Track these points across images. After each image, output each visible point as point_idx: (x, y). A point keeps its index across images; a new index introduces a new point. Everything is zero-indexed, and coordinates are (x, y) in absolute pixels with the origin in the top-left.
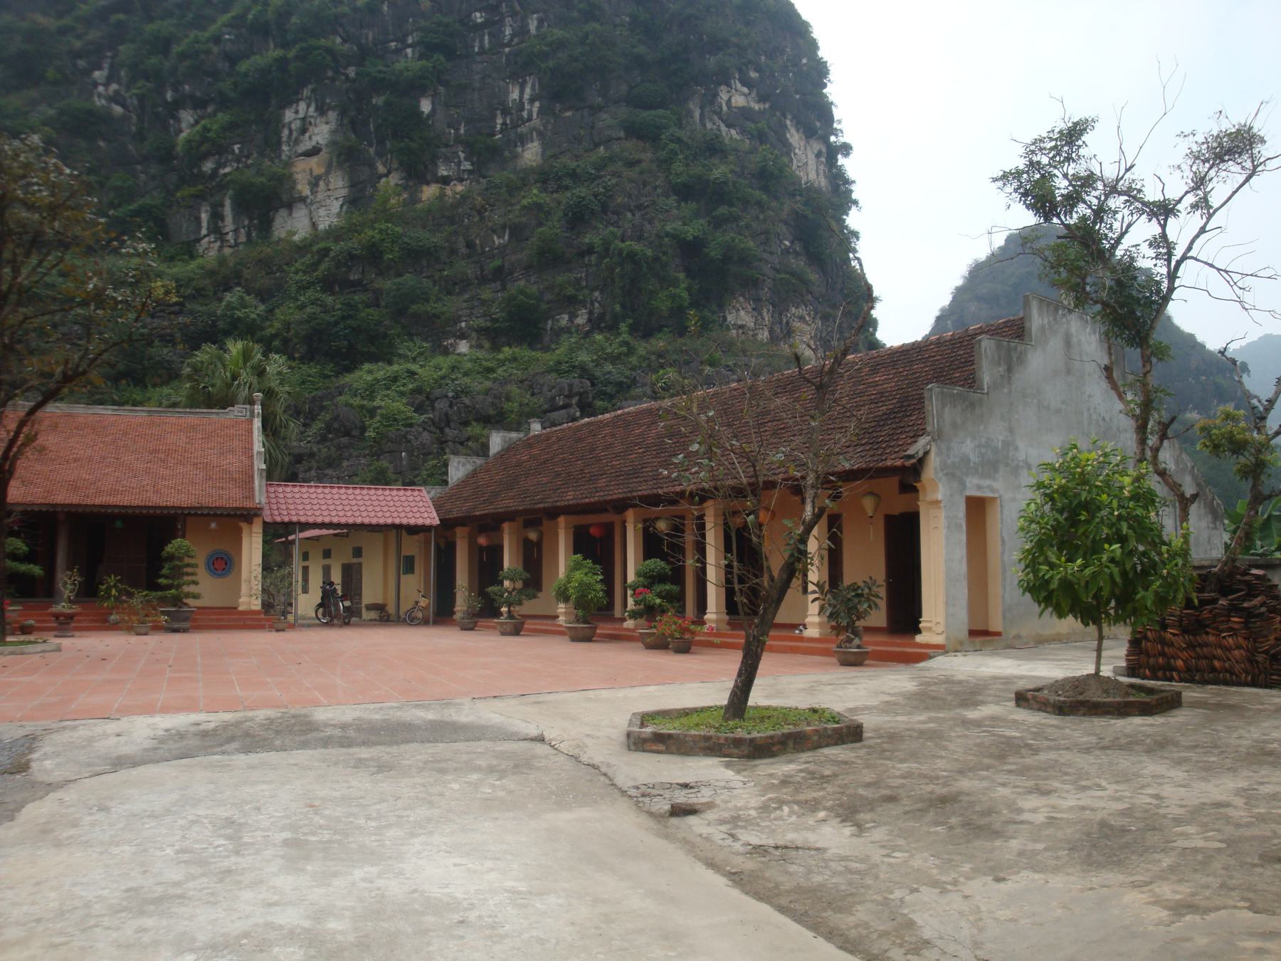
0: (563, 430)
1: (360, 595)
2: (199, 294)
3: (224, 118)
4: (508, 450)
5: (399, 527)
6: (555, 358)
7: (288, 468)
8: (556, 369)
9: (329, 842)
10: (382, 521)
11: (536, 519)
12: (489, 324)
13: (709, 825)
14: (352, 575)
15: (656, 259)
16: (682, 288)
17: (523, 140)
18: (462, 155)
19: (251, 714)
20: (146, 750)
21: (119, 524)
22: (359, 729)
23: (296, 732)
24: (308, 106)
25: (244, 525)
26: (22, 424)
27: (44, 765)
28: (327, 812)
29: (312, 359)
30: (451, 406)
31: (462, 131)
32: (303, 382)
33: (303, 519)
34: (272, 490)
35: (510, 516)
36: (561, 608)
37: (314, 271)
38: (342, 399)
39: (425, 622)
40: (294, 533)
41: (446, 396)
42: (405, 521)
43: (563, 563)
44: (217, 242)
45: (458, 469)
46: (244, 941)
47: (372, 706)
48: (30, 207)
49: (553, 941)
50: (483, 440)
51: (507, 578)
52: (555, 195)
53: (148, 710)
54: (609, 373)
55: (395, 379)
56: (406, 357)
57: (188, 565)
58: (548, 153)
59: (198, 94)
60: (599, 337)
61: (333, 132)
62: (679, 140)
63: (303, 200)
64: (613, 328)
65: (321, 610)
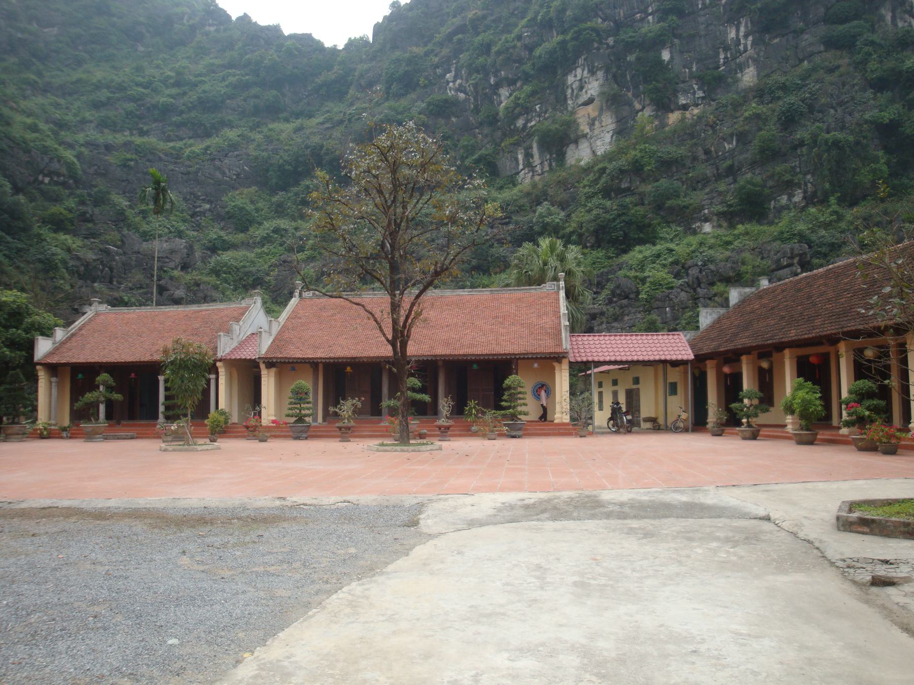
0: (786, 284)
1: (639, 411)
2: (520, 209)
3: (528, 88)
4: (744, 302)
5: (664, 362)
6: (778, 229)
7: (585, 324)
8: (781, 238)
9: (605, 585)
10: (652, 358)
11: (768, 351)
12: (725, 209)
13: (905, 595)
14: (632, 397)
15: (857, 143)
16: (882, 161)
17: (741, 67)
18: (696, 87)
19: (558, 494)
20: (490, 516)
21: (475, 366)
22: (632, 507)
23: (589, 507)
24: (583, 71)
25: (556, 364)
26: (413, 305)
27: (427, 523)
28: (605, 564)
29: (599, 247)
30: (701, 272)
31: (694, 69)
32: (594, 263)
33: (596, 359)
34: (574, 339)
35: (747, 351)
36: (789, 419)
37: (596, 185)
38: (621, 273)
39: (686, 430)
40: (590, 369)
41: (697, 265)
42: (668, 358)
43: (789, 384)
44: (529, 173)
45: (706, 318)
46: (541, 649)
47: (642, 491)
48: (410, 167)
49: (764, 675)
50: (725, 295)
51: (746, 397)
52: (770, 105)
53: (492, 489)
54: (823, 237)
55: (658, 256)
56: (665, 239)
57: (520, 393)
58: (762, 74)
59: (510, 76)
60: (813, 210)
61: (602, 86)
62: (872, 43)
63: (585, 136)
64: (824, 201)
65: (612, 422)
